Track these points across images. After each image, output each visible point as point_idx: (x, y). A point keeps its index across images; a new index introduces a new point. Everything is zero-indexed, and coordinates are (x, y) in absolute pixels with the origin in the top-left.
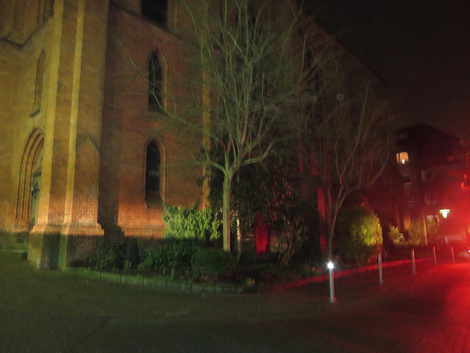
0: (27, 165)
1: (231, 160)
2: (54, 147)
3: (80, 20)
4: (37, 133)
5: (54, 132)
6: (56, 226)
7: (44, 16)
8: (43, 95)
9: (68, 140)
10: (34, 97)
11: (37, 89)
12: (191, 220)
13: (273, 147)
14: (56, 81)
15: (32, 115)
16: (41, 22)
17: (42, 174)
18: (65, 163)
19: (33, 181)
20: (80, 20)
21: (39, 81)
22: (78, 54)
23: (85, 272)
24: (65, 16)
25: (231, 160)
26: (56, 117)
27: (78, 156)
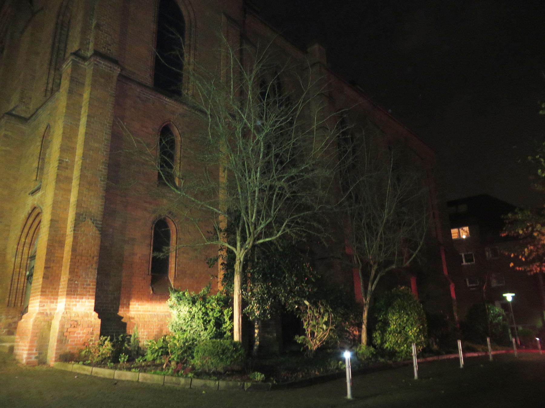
0: (24, 247)
1: (244, 239)
2: (50, 227)
3: (86, 96)
4: (36, 211)
5: (52, 213)
6: (47, 314)
7: (52, 90)
8: (45, 170)
9: (67, 219)
10: (36, 174)
11: (40, 166)
12: (199, 308)
13: (288, 226)
14: (57, 158)
15: (33, 193)
16: (49, 94)
17: (37, 257)
18: (62, 244)
19: (30, 264)
20: (86, 96)
21: (42, 158)
22: (82, 130)
23: (75, 367)
24: (70, 92)
25: (244, 239)
26: (55, 195)
27: (75, 237)
